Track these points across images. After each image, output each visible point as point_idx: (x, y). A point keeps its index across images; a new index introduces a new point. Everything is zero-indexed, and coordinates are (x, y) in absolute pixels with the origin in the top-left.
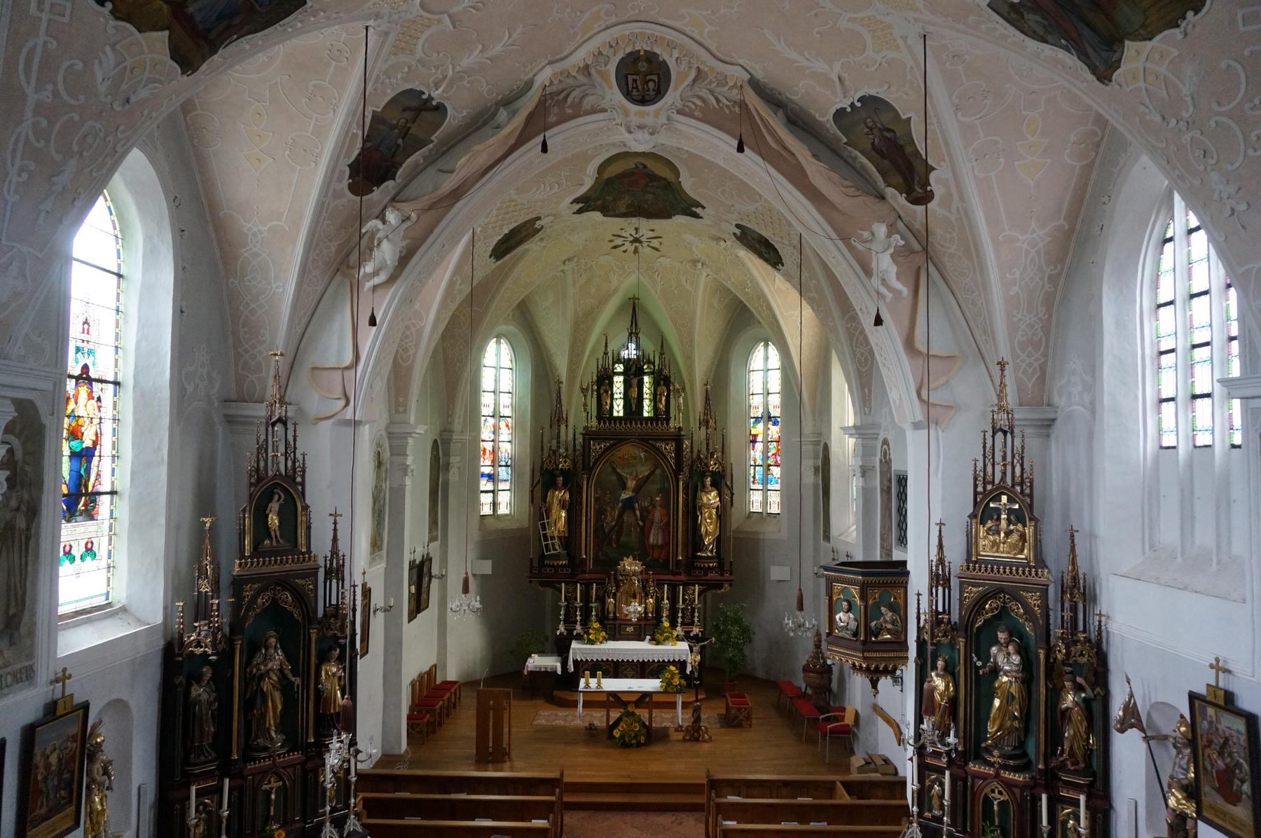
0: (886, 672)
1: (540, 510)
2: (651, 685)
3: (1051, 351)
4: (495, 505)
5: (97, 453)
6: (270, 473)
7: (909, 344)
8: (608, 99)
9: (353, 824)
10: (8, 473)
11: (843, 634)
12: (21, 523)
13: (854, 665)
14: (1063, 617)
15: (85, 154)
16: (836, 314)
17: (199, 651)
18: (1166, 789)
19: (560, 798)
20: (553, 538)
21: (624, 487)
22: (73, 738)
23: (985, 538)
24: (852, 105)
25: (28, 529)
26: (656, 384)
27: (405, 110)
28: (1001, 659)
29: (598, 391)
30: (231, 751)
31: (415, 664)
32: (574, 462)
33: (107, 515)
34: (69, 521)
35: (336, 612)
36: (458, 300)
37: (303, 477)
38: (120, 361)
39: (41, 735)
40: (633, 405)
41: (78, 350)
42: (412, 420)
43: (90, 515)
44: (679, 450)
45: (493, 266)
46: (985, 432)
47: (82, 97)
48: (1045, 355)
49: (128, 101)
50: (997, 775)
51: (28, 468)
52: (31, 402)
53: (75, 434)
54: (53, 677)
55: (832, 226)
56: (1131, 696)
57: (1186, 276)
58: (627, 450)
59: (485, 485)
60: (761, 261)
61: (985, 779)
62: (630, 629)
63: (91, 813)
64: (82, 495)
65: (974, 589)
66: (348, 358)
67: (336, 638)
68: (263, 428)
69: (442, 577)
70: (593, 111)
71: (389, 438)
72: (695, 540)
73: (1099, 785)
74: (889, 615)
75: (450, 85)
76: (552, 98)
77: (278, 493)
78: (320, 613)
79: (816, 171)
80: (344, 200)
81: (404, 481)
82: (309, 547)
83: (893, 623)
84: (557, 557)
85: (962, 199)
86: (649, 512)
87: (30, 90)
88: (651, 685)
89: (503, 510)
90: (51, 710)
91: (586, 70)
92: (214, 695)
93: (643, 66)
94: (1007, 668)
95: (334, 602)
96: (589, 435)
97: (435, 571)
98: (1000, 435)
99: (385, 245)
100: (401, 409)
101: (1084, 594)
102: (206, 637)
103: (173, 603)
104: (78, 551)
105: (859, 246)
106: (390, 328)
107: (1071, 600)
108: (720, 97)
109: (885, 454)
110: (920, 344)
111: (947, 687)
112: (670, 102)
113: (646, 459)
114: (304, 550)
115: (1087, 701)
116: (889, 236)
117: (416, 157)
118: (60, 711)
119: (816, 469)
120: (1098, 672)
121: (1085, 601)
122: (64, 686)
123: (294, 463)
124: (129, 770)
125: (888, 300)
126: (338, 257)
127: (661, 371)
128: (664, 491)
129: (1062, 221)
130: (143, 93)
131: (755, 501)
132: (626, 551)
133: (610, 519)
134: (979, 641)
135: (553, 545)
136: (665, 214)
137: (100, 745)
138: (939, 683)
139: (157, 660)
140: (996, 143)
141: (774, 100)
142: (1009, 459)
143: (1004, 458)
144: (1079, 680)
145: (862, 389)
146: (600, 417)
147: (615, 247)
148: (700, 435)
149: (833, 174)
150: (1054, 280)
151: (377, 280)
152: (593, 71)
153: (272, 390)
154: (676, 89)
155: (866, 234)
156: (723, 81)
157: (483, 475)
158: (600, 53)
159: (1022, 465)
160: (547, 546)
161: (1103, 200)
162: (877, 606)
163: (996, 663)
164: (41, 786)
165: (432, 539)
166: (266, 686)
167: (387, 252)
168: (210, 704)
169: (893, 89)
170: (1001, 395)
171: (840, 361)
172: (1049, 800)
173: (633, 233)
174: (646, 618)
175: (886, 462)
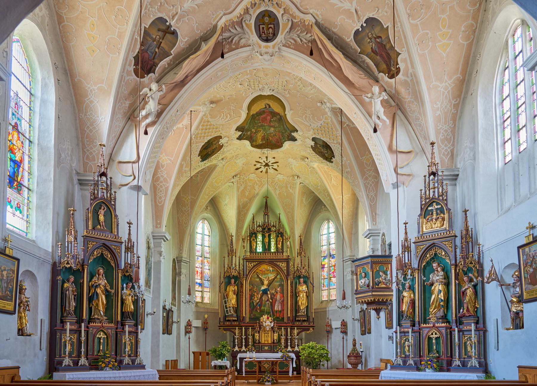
1: (225, 297)
3: (456, 143)
4: (202, 297)
5: (22, 166)
6: (100, 196)
17: (68, 266)
20: (230, 307)
21: (263, 284)
27: (159, 30)
32: (239, 273)
37: (115, 202)
40: (266, 248)
48: (453, 145)
50: (434, 326)
57: (514, 78)
58: (264, 267)
59: (197, 288)
62: (266, 348)
65: (422, 247)
66: (134, 158)
69: (178, 322)
70: (244, 46)
72: (296, 308)
76: (226, 41)
77: (104, 207)
78: (123, 267)
80: (131, 78)
84: (232, 316)
85: (413, 67)
86: (274, 296)
89: (206, 301)
93: (267, 19)
95: (129, 262)
96: (246, 259)
97: (175, 319)
100: (159, 226)
110: (394, 148)
113: (273, 271)
116: (380, 93)
123: (111, 195)
126: (129, 115)
128: (281, 286)
129: (459, 75)
131: (324, 295)
133: (256, 299)
134: (425, 269)
140: (427, 34)
145: (372, 213)
146: (251, 252)
147: (257, 169)
150: (456, 106)
154: (282, 34)
155: (369, 95)
157: (197, 283)
160: (227, 311)
162: (378, 272)
167: (152, 106)
169: (380, 11)
173: (265, 160)
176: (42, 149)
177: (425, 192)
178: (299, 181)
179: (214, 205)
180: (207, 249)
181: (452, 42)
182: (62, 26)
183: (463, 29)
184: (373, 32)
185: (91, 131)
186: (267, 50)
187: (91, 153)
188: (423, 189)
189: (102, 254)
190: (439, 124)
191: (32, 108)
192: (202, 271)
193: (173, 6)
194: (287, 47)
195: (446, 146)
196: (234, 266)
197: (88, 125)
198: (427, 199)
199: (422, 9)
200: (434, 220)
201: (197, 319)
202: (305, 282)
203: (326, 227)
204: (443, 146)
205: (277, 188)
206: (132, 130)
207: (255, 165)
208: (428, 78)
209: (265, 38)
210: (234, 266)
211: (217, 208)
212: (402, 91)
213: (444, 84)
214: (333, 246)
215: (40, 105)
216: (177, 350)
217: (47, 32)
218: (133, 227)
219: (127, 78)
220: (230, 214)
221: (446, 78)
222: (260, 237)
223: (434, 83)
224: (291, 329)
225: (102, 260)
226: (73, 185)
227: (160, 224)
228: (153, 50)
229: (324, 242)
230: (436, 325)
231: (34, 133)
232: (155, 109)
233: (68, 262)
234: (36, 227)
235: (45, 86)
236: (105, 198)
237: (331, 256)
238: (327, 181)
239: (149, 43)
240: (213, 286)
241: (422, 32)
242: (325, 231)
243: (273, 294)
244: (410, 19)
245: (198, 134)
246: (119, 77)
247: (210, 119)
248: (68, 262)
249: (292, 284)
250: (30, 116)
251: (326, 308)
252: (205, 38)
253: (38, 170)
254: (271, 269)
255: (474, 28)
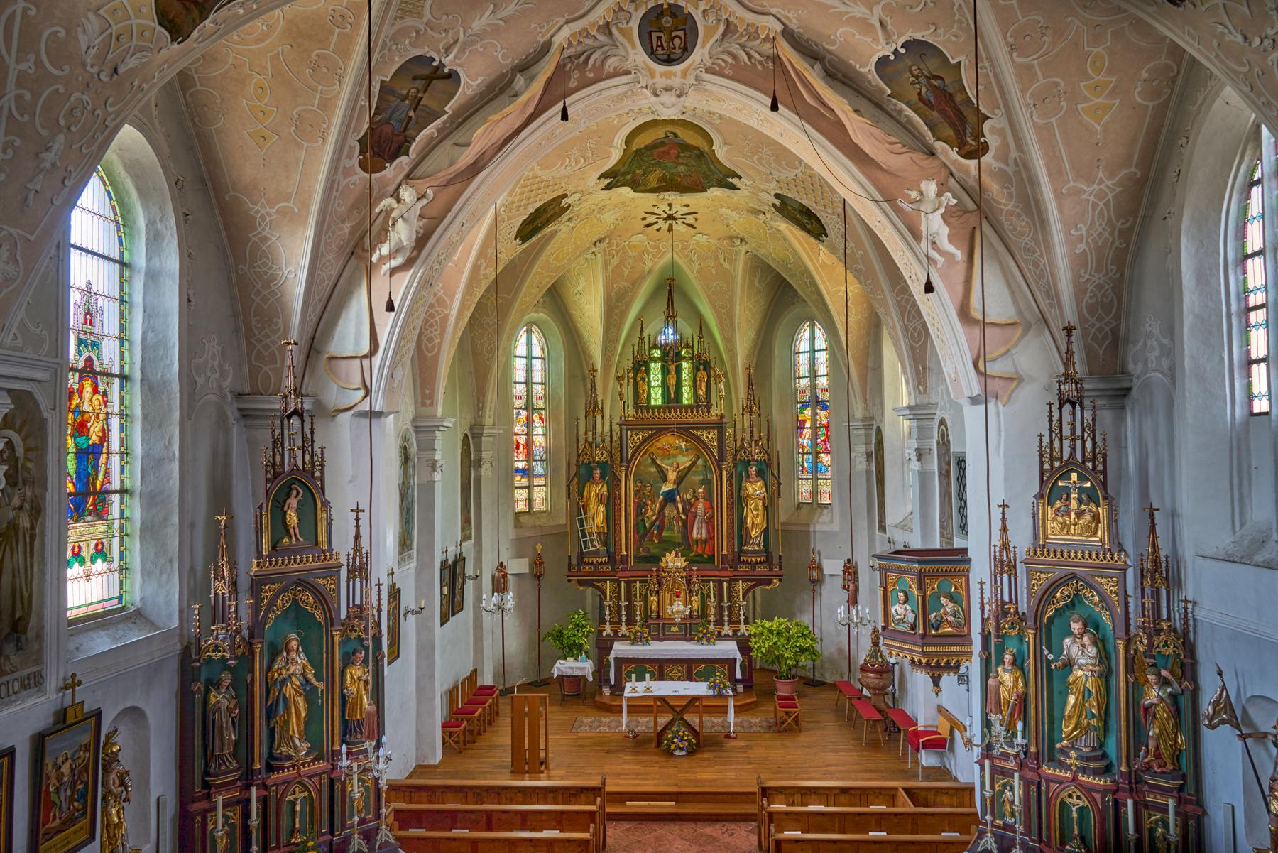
0: (949, 668)
2: (699, 688)
4: (530, 501)
5: (104, 450)
6: (287, 468)
7: (964, 313)
8: (631, 58)
9: (384, 835)
10: (6, 468)
11: (899, 627)
12: (24, 522)
13: (913, 661)
14: (1143, 604)
15: (73, 129)
16: (885, 285)
17: (217, 656)
18: (1267, 792)
19: (602, 807)
20: (591, 534)
21: (665, 479)
22: (86, 747)
23: (1053, 520)
24: (896, 52)
25: (33, 528)
26: (695, 370)
27: (415, 79)
28: (1075, 652)
29: (635, 378)
30: (253, 761)
31: (449, 669)
32: (611, 454)
33: (117, 515)
34: (76, 522)
35: (359, 612)
36: (485, 285)
37: (322, 471)
38: (126, 354)
39: (51, 745)
41: (80, 342)
42: (440, 411)
43: (101, 514)
44: (721, 439)
45: (520, 249)
46: (1050, 404)
47: (67, 68)
48: (1117, 317)
49: (116, 71)
50: (1074, 779)
51: (30, 465)
52: (29, 393)
53: (81, 428)
54: (61, 684)
55: (874, 184)
56: (1224, 688)
58: (667, 440)
59: (519, 481)
60: (803, 233)
61: (1061, 783)
62: (675, 629)
63: (108, 825)
64: (90, 494)
65: (1043, 576)
66: (365, 349)
67: (360, 640)
68: (278, 422)
70: (615, 74)
71: (416, 432)
72: (741, 534)
73: (1190, 788)
74: (949, 607)
75: (462, 50)
78: (343, 615)
79: (859, 128)
81: (432, 477)
82: (330, 545)
83: (954, 615)
84: (596, 554)
86: (691, 505)
87: (11, 61)
88: (699, 688)
90: (62, 720)
91: (606, 28)
92: (234, 701)
93: (667, 21)
94: (1082, 661)
96: (627, 425)
97: (469, 571)
98: (1067, 407)
99: (400, 224)
101: (1167, 578)
102: (224, 640)
103: (189, 606)
104: (87, 552)
105: (907, 207)
106: (409, 313)
107: (1152, 586)
108: (752, 53)
109: (943, 434)
111: (1016, 681)
112: (699, 61)
114: (325, 548)
115: (1174, 697)
116: (939, 195)
117: (430, 130)
118: (70, 720)
119: (869, 455)
120: (1187, 667)
121: (1168, 586)
122: (73, 692)
123: (312, 457)
124: (147, 782)
125: (939, 265)
127: (699, 356)
128: (707, 482)
130: (132, 63)
132: (667, 545)
133: (650, 515)
134: (1049, 632)
135: (592, 541)
136: (698, 187)
137: (116, 754)
138: (1007, 678)
139: (175, 665)
140: (1057, 84)
141: (812, 53)
142: (1078, 433)
143: (1073, 431)
144: (1164, 673)
146: (637, 406)
147: (648, 226)
148: (744, 422)
149: (877, 132)
150: (1125, 234)
151: (394, 263)
152: (614, 31)
153: (288, 382)
154: (703, 47)
155: (914, 194)
156: (753, 33)
157: (517, 470)
158: (621, 9)
159: (1093, 439)
160: (585, 542)
161: (1180, 142)
162: (937, 596)
163: (1069, 656)
164: (54, 797)
165: (466, 538)
166: (288, 691)
167: (402, 233)
168: (230, 711)
169: (940, 31)
170: (1068, 363)
171: (892, 337)
172: (1136, 804)
173: (667, 209)
174: (691, 616)
175: (944, 443)
176: (151, 389)
177: (1052, 441)
178: (743, 248)
179: (557, 300)
180: (538, 389)
181: (1117, 101)
182: (191, 95)
183: (1145, 75)
184: (922, 66)
185: (265, 300)
186: (669, 82)
187: (267, 347)
188: (1047, 433)
189: (295, 601)
190: (1082, 272)
191: (126, 298)
192: (527, 441)
193: (446, 31)
194: (714, 73)
195: (1099, 319)
196: (599, 439)
197: (259, 286)
198: (1057, 460)
199: (1043, 35)
200: (1073, 516)
201: (519, 556)
202: (760, 474)
203: (807, 335)
204: (1092, 321)
205: (695, 259)
206: (360, 284)
207: (644, 219)
208: (1056, 173)
209: (665, 57)
210: (599, 439)
211: (560, 296)
212: (993, 187)
213: (1095, 186)
214: (823, 382)
215: (145, 286)
216: (475, 634)
217: (156, 121)
218: (364, 517)
219: (343, 183)
220: (590, 310)
221: (1101, 174)
222: (655, 367)
223: (1072, 184)
224: (729, 583)
225: (298, 615)
226: (227, 431)
227: (431, 396)
228: (403, 116)
229: (804, 370)
230: (1080, 777)
231: (131, 357)
232: (409, 239)
233: (217, 646)
234: (142, 574)
235: (154, 239)
236: (298, 469)
237: (817, 403)
238: (809, 256)
239: (393, 105)
240: (552, 473)
241: (1042, 81)
242: (804, 345)
243: (688, 501)
244: (1015, 54)
245: (513, 203)
246: (326, 185)
247: (539, 173)
248: (217, 646)
249: (730, 479)
250: (122, 316)
251: (808, 525)
252: (526, 66)
253: (142, 441)
254: (683, 445)
255: (1171, 75)
